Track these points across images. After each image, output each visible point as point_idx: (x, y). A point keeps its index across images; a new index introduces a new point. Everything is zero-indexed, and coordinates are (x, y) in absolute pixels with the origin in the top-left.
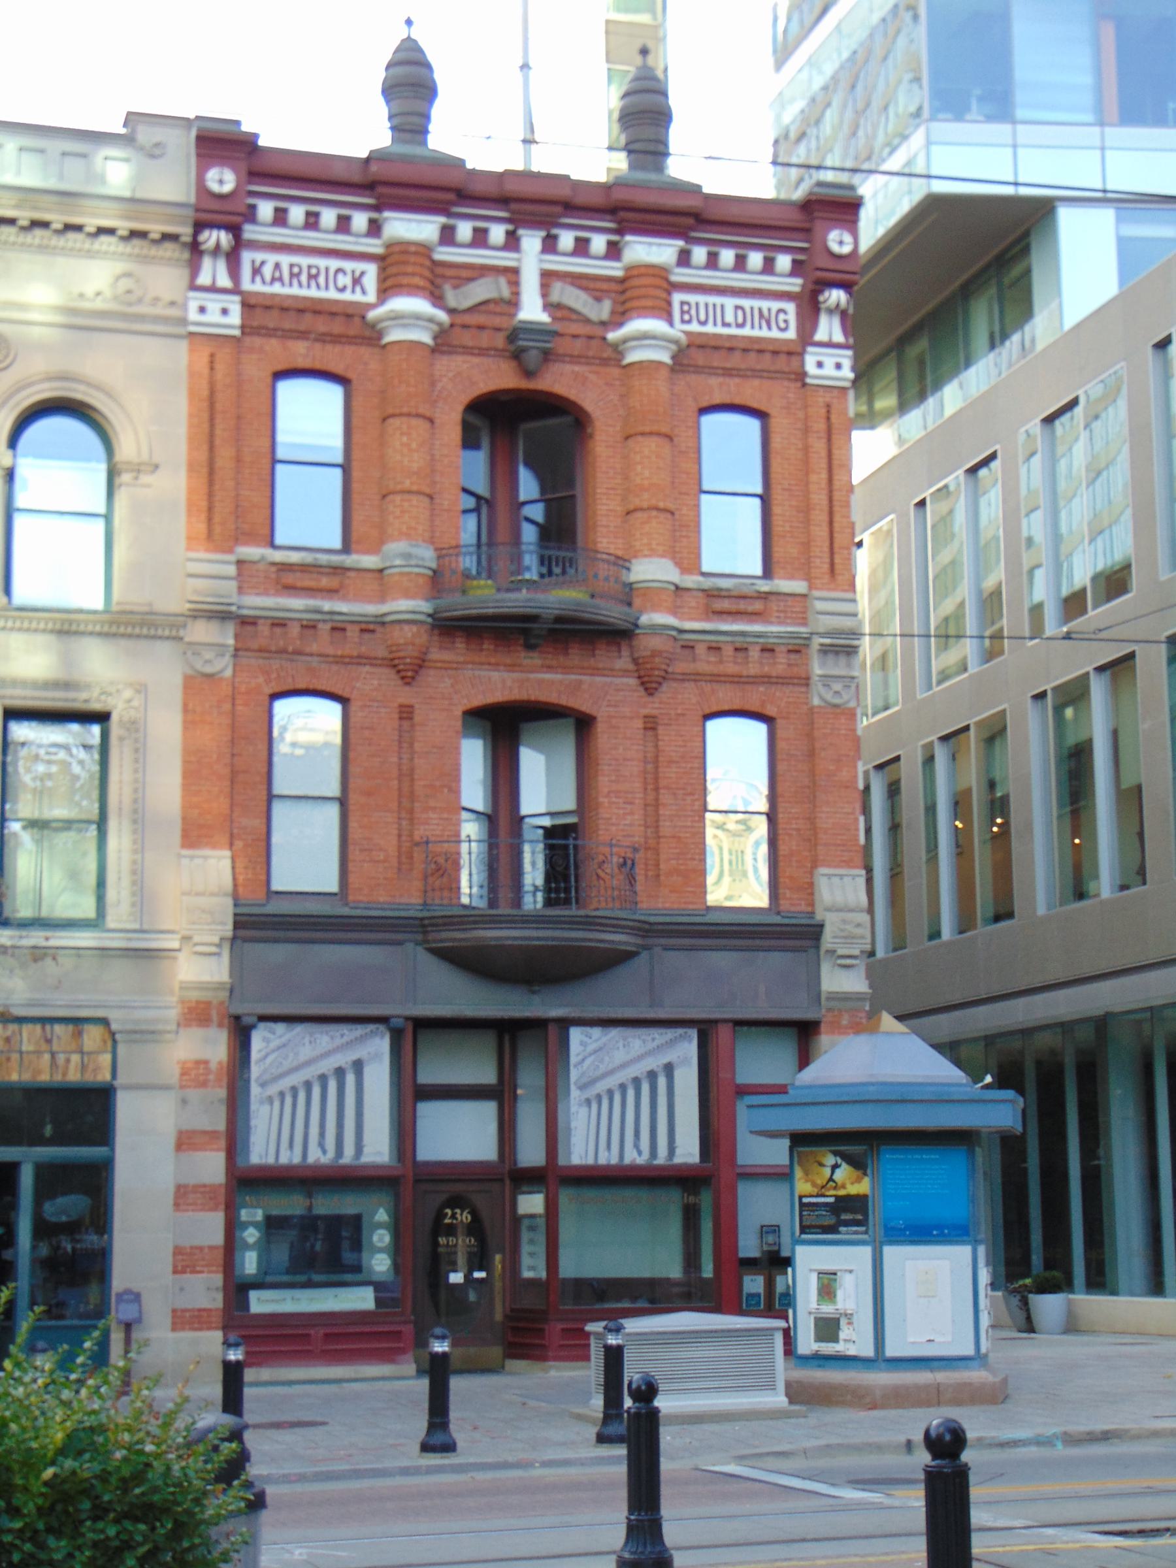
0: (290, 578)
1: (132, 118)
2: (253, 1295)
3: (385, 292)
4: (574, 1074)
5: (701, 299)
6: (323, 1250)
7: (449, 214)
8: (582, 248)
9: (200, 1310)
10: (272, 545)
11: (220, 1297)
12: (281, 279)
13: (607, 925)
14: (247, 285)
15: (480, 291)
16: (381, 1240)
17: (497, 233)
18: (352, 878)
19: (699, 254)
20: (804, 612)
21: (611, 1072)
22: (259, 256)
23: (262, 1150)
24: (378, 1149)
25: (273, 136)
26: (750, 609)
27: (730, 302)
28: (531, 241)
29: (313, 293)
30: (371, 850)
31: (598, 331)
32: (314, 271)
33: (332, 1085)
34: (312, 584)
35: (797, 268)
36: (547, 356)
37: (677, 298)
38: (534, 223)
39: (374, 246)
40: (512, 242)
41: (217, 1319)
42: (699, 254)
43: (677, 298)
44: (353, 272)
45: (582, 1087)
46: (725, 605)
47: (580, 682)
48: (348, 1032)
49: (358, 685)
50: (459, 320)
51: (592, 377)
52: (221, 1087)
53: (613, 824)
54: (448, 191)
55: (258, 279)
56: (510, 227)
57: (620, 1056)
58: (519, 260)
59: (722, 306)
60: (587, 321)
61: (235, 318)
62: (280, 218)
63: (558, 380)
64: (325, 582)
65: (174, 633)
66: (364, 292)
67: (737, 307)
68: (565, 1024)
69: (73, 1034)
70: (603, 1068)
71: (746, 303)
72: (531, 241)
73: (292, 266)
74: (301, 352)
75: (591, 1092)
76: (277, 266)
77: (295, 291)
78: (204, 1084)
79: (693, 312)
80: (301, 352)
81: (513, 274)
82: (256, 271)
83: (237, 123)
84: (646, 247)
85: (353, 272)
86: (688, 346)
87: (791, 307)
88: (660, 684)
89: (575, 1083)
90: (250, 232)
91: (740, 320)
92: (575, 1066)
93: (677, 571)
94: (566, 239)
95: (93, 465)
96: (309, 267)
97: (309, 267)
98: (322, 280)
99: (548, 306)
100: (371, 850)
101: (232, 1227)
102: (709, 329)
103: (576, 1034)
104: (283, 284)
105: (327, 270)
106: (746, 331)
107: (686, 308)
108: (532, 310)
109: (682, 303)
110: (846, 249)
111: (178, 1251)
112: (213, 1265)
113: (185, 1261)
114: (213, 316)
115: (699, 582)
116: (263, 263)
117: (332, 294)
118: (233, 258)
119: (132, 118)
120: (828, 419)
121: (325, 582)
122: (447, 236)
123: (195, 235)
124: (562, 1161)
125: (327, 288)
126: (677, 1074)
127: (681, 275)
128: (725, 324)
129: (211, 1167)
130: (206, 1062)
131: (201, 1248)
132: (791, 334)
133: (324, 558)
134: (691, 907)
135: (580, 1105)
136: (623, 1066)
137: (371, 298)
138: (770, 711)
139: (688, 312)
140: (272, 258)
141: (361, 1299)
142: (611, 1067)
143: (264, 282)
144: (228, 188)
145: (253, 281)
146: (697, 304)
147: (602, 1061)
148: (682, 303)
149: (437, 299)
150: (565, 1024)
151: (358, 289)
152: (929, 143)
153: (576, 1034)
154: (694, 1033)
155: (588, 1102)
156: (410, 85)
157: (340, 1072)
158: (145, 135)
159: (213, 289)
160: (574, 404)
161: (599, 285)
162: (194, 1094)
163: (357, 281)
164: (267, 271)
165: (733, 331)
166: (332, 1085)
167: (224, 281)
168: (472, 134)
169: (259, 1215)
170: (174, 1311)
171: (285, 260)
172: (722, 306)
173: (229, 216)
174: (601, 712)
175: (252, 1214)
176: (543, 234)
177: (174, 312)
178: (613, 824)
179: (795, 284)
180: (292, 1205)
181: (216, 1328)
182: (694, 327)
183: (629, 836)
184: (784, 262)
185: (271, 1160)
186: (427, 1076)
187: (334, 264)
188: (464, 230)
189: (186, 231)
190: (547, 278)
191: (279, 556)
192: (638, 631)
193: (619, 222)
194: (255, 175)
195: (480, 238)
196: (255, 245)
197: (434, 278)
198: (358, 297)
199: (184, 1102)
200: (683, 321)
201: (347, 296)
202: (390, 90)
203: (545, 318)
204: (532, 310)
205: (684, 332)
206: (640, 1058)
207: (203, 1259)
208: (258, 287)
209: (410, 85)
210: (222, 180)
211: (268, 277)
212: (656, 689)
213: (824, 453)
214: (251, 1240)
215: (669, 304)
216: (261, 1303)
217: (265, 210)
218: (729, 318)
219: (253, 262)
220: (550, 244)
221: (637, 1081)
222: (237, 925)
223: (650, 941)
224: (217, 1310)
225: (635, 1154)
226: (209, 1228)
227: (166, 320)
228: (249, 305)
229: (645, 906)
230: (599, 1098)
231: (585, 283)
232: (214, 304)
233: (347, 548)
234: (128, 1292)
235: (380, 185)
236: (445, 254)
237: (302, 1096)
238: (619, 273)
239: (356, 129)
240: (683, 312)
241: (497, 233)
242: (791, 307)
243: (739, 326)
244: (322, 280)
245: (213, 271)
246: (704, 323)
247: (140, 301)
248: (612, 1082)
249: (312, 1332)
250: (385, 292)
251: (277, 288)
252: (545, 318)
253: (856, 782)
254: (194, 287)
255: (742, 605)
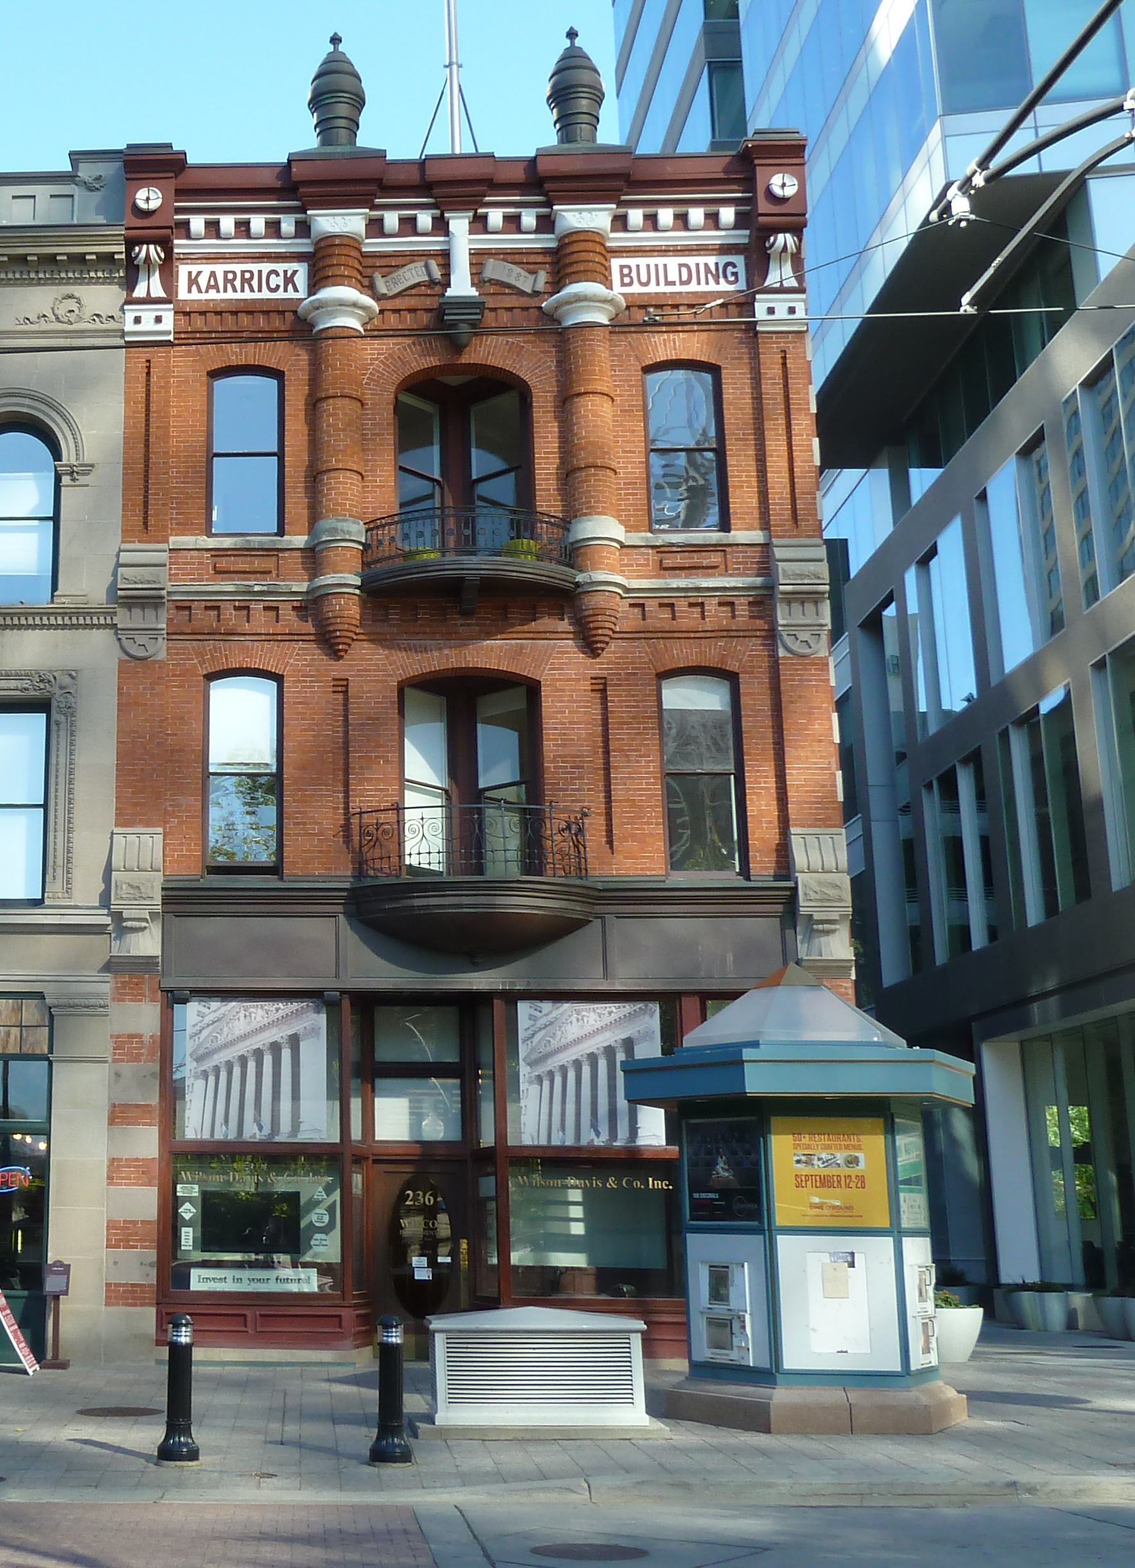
0: (223, 563)
1: (76, 157)
2: (195, 1273)
3: (314, 285)
4: (523, 1050)
5: (643, 261)
6: (254, 1225)
7: (373, 207)
8: (513, 223)
9: (133, 1285)
10: (210, 535)
11: (153, 1272)
12: (216, 287)
13: (512, 889)
14: (183, 294)
15: (414, 274)
16: (320, 1220)
17: (425, 220)
18: (287, 851)
19: (636, 216)
20: (768, 562)
21: (231, 1043)
22: (195, 269)
23: (197, 1123)
24: (317, 1122)
25: (202, 151)
26: (705, 563)
27: (673, 262)
28: (459, 224)
29: (247, 295)
30: (304, 824)
31: (533, 302)
32: (247, 276)
33: (268, 1060)
34: (246, 567)
35: (741, 221)
36: (478, 329)
37: (615, 263)
38: (460, 205)
39: (303, 246)
40: (441, 226)
41: (151, 1295)
42: (636, 216)
43: (615, 263)
44: (285, 272)
45: (532, 1064)
46: (679, 560)
47: (522, 647)
48: (283, 1008)
49: (291, 661)
50: (389, 305)
51: (529, 346)
52: (154, 1061)
53: (561, 790)
54: (366, 181)
55: (194, 288)
56: (437, 212)
57: (241, 1026)
58: (448, 242)
59: (665, 266)
60: (521, 293)
61: (168, 323)
62: (213, 228)
63: (488, 352)
64: (257, 564)
65: (109, 621)
66: (296, 290)
67: (681, 266)
68: (512, 998)
69: (13, 1008)
70: (222, 1040)
71: (691, 261)
72: (459, 224)
73: (226, 273)
74: (236, 354)
75: (541, 1070)
76: (213, 274)
77: (230, 295)
78: (137, 1058)
79: (634, 274)
80: (236, 354)
81: (445, 258)
82: (193, 281)
83: (170, 146)
84: (576, 214)
85: (285, 272)
86: (628, 307)
87: (739, 260)
88: (607, 643)
89: (524, 1060)
90: (181, 245)
91: (685, 278)
92: (524, 1041)
93: (623, 528)
94: (495, 217)
95: (46, 474)
96: (243, 272)
97: (243, 272)
98: (255, 283)
99: (478, 279)
100: (304, 824)
101: (170, 1204)
102: (652, 288)
103: (523, 1008)
104: (218, 291)
105: (260, 272)
106: (693, 287)
107: (626, 271)
108: (461, 286)
109: (622, 267)
110: (790, 192)
111: (112, 1225)
112: (146, 1241)
113: (121, 1234)
114: (148, 324)
115: (647, 539)
116: (199, 273)
117: (265, 294)
118: (168, 267)
119: (76, 157)
120: (784, 364)
121: (257, 564)
122: (376, 227)
123: (129, 251)
124: (511, 1142)
125: (260, 290)
126: (303, 1045)
127: (617, 239)
128: (667, 283)
129: (146, 1143)
130: (140, 1036)
131: (134, 1223)
132: (742, 285)
133: (256, 541)
134: (648, 873)
135: (531, 1083)
136: (244, 1037)
137: (302, 294)
138: (732, 666)
139: (629, 275)
140: (206, 269)
141: (309, 1282)
142: (230, 1038)
143: (200, 291)
144: (154, 204)
145: (190, 291)
146: (638, 266)
147: (221, 1032)
148: (622, 267)
149: (370, 288)
150: (512, 998)
151: (290, 287)
152: (945, 137)
153: (523, 1008)
154: (656, 1008)
155: (539, 1079)
156: (336, 93)
157: (275, 1048)
158: (86, 172)
159: (149, 300)
160: (525, 383)
161: (532, 258)
162: (126, 1068)
163: (289, 280)
164: (203, 281)
165: (678, 288)
166: (268, 1060)
167: (158, 291)
168: (392, 130)
169: (195, 1191)
170: (108, 1285)
171: (220, 269)
172: (665, 266)
173: (164, 233)
174: (545, 676)
175: (189, 1190)
176: (471, 214)
177: (112, 325)
178: (561, 790)
179: (742, 236)
180: (244, 1182)
181: (151, 1305)
182: (636, 289)
183: (580, 801)
184: (727, 214)
185: (206, 1136)
186: (387, 1051)
187: (266, 267)
188: (391, 220)
189: (118, 249)
190: (478, 258)
191: (212, 543)
192: (580, 590)
193: (546, 195)
194: (181, 193)
195: (409, 226)
196: (188, 258)
197: (370, 272)
198: (291, 294)
199: (118, 1075)
200: (623, 284)
201: (280, 295)
202: (317, 102)
203: (473, 292)
204: (461, 286)
205: (624, 295)
206: (261, 1029)
207: (136, 1234)
208: (195, 295)
209: (336, 93)
210: (149, 197)
211: (203, 287)
212: (603, 649)
213: (780, 398)
214: (187, 1216)
215: (608, 269)
216: (200, 1281)
217: (197, 223)
218: (673, 276)
219: (190, 273)
220: (480, 224)
221: (258, 1054)
222: (166, 901)
223: (598, 909)
224: (150, 1286)
225: (256, 1129)
226: (144, 1203)
227: (106, 333)
228: (183, 312)
229: (597, 873)
230: (551, 1074)
231: (517, 258)
232: (148, 315)
233: (281, 532)
234: (58, 1263)
235: (294, 187)
236: (373, 245)
237: (237, 1071)
238: (553, 245)
239: (288, 134)
240: (622, 276)
241: (425, 220)
242: (739, 260)
243: (682, 283)
244: (255, 283)
245: (151, 285)
246: (647, 284)
247: (80, 319)
248: (566, 1058)
249: (247, 1313)
250: (314, 285)
251: (212, 295)
252: (473, 292)
253: (832, 736)
254: (130, 301)
255: (696, 559)
